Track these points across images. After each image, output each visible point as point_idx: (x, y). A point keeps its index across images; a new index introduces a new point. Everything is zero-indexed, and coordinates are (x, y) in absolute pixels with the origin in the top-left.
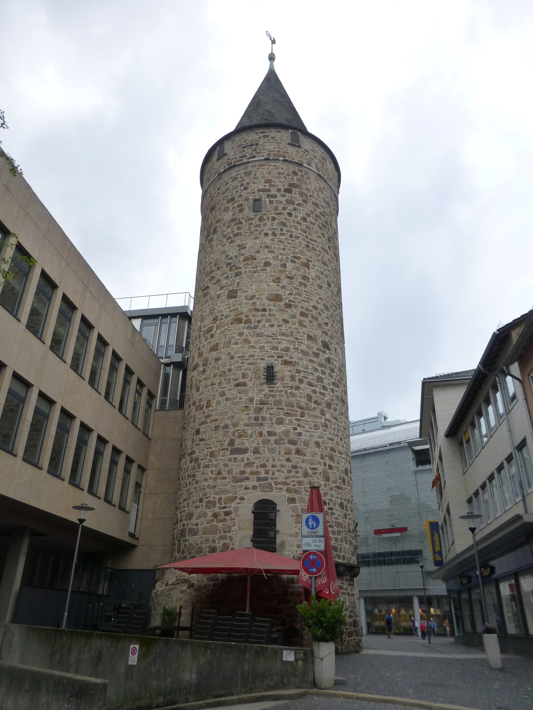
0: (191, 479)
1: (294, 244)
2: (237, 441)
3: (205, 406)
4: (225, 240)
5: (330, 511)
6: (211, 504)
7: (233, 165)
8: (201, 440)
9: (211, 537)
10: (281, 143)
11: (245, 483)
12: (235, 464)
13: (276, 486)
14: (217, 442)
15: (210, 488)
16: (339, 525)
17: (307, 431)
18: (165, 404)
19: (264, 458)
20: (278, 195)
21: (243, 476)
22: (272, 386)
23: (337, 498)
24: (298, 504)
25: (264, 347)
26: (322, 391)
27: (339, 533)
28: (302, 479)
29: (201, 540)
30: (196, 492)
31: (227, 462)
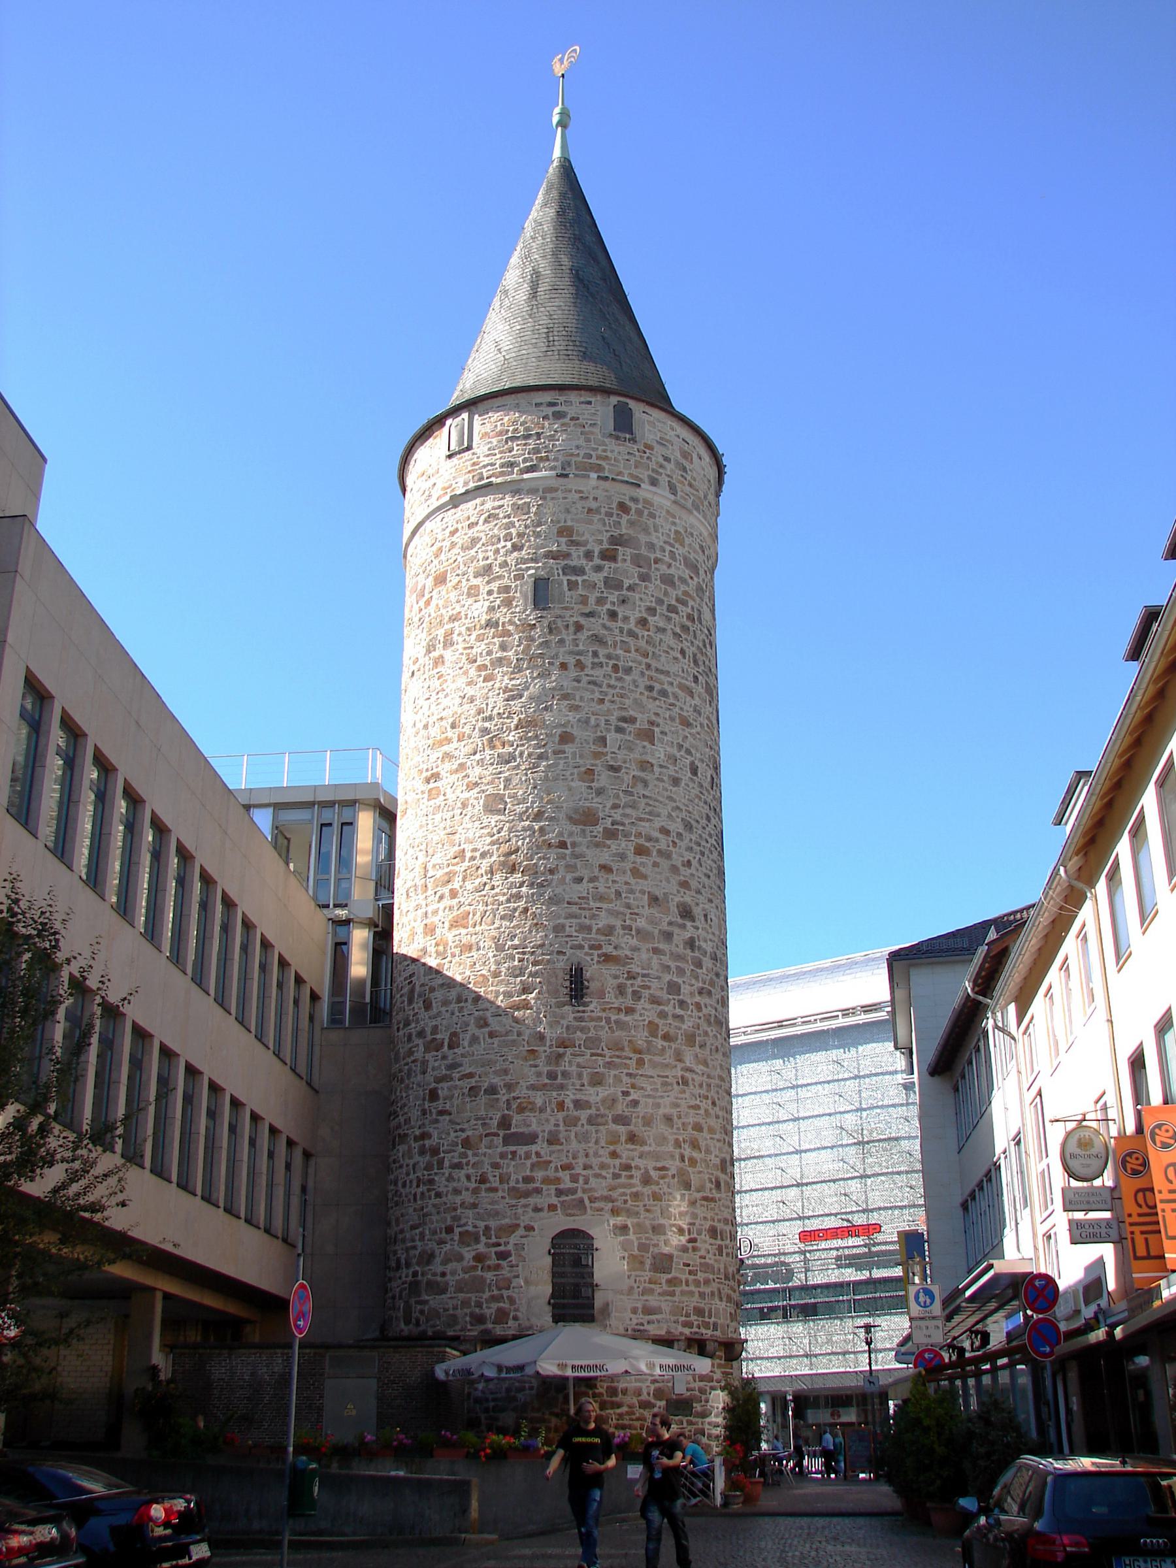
0: (425, 1188)
1: (622, 688)
2: (516, 1119)
3: (446, 1044)
4: (473, 672)
5: (690, 1245)
6: (469, 1238)
7: (486, 481)
8: (442, 1113)
9: (473, 1297)
10: (592, 433)
11: (533, 1200)
12: (513, 1163)
13: (593, 1205)
14: (476, 1119)
15: (466, 1208)
16: (706, 1267)
17: (649, 1096)
18: (343, 1013)
19: (568, 1152)
20: (588, 566)
21: (531, 1186)
22: (581, 1008)
23: (705, 1218)
24: (632, 1236)
25: (563, 926)
26: (679, 1011)
27: (707, 1282)
28: (639, 1188)
29: (455, 1302)
30: (438, 1213)
31: (498, 1160)
